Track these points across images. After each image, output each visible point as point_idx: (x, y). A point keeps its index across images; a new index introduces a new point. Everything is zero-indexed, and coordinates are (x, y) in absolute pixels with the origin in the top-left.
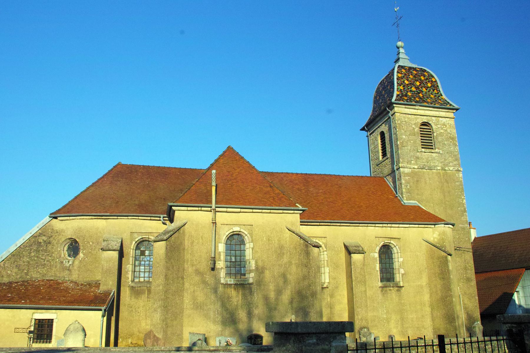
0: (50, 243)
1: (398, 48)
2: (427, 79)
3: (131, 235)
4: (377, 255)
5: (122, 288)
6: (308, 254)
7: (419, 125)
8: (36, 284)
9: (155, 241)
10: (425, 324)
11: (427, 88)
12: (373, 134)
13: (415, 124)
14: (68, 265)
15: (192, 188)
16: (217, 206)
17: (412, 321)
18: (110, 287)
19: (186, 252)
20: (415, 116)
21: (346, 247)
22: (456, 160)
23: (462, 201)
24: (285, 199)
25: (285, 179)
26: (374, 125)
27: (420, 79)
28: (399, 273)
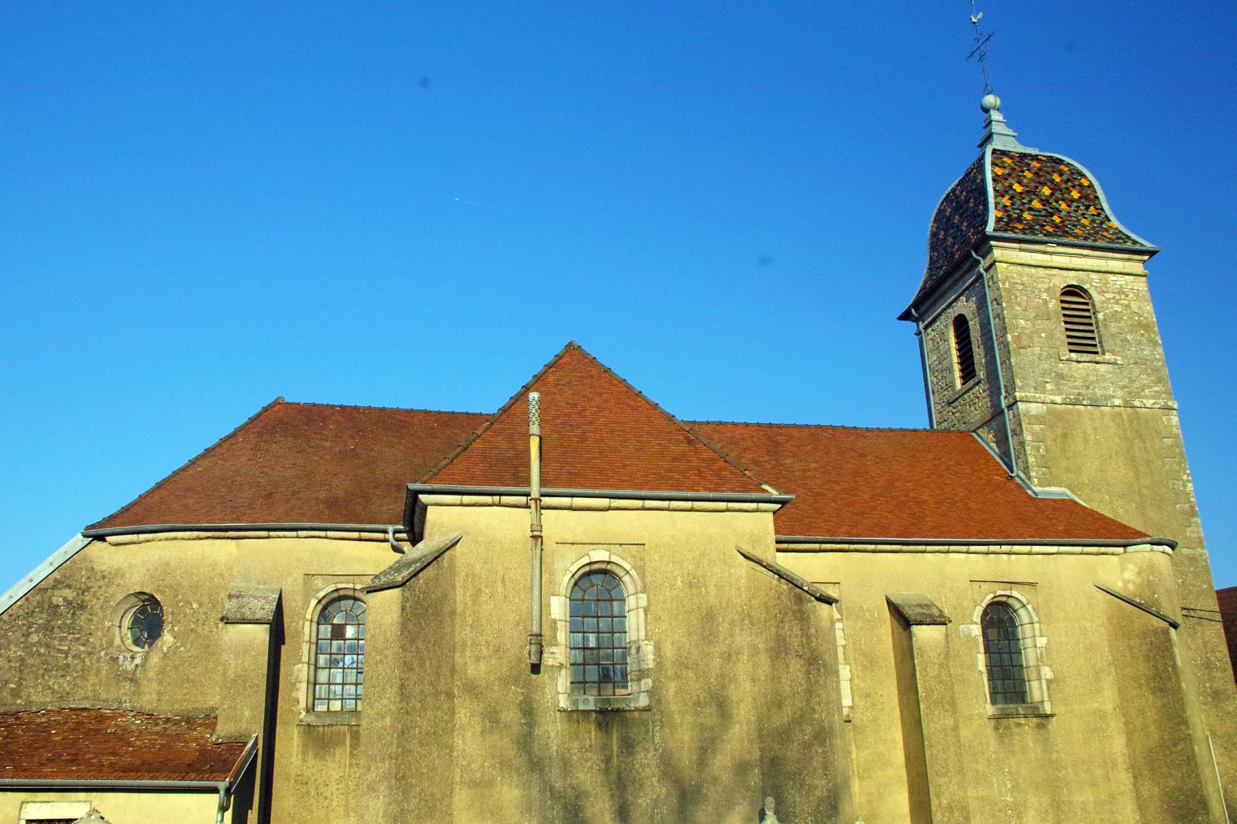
0: (82, 607)
1: (986, 110)
2: (1068, 180)
3: (305, 582)
4: (976, 630)
5: (279, 730)
6: (803, 618)
7: (1059, 293)
8: (38, 721)
9: (371, 590)
10: (1120, 818)
11: (1070, 202)
12: (934, 326)
13: (1048, 290)
14: (130, 666)
15: (474, 445)
16: (545, 490)
17: (1084, 810)
18: (244, 725)
19: (458, 621)
20: (1047, 271)
21: (896, 610)
22: (1159, 381)
23: (1185, 486)
24: (731, 473)
25: (716, 436)
26: (936, 301)
27: (1052, 181)
28: (1039, 679)
